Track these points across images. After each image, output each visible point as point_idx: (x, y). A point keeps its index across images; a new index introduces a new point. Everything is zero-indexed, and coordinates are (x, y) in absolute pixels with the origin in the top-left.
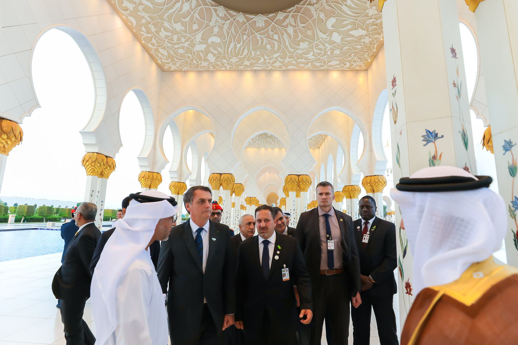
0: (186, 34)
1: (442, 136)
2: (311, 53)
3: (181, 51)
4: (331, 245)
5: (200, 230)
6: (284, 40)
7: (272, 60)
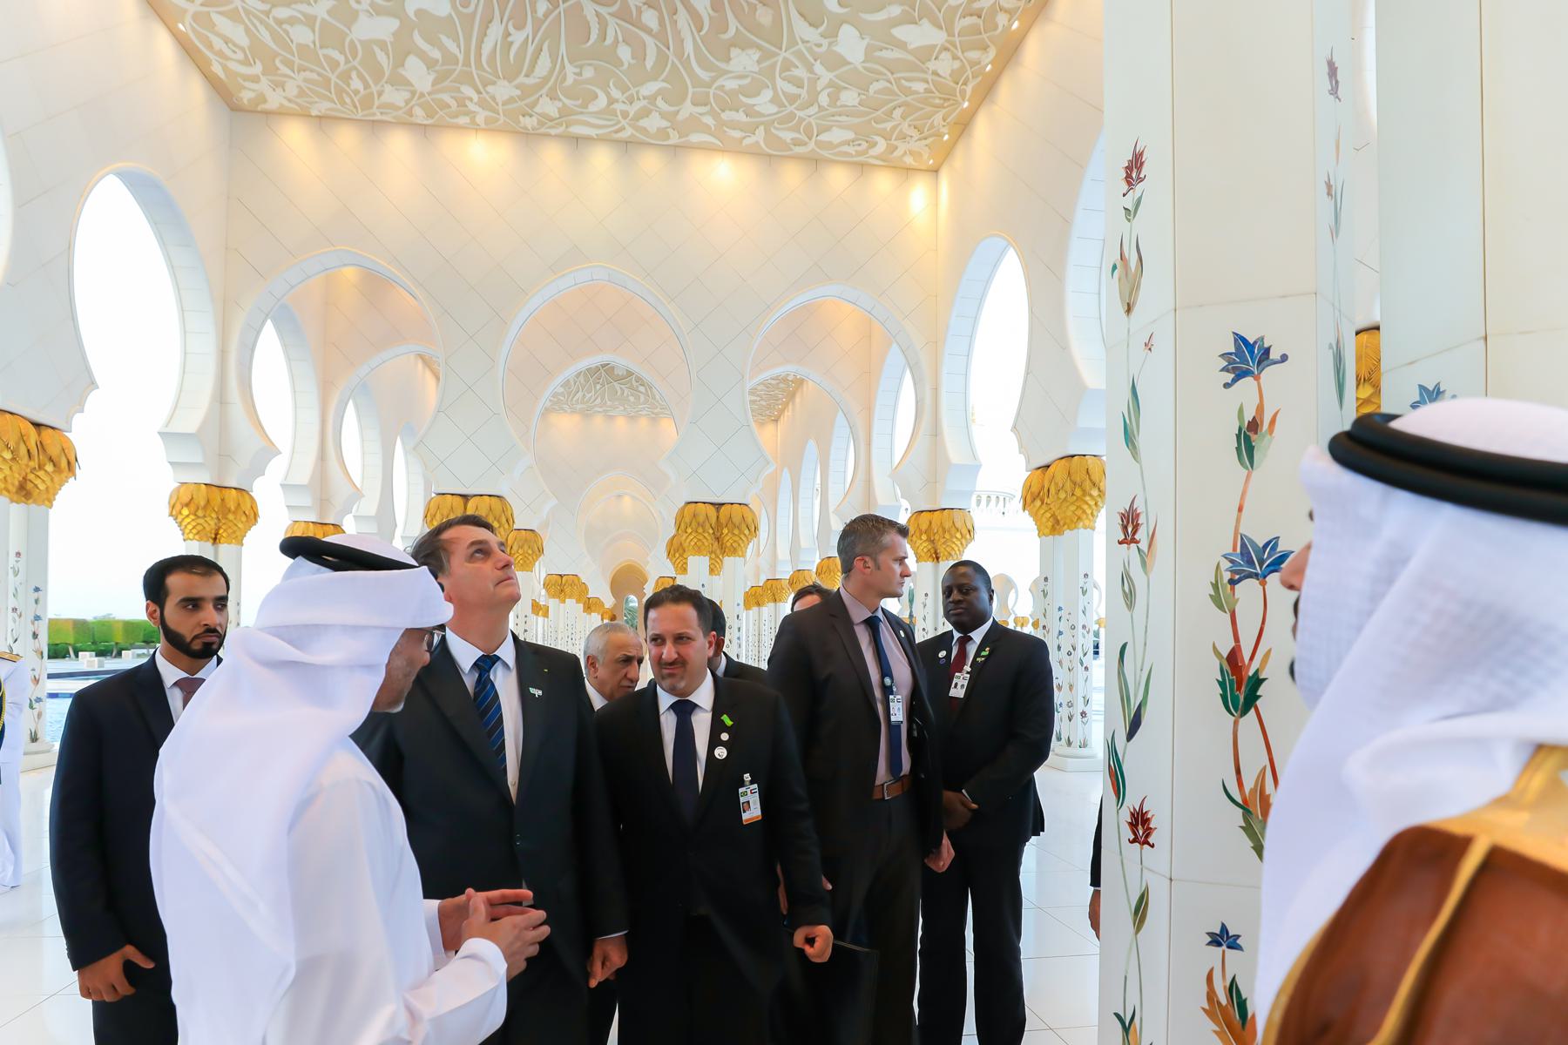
1: (1284, 358)
2: (767, 94)
4: (898, 712)
5: (486, 664)
6: (677, 33)
7: (638, 105)
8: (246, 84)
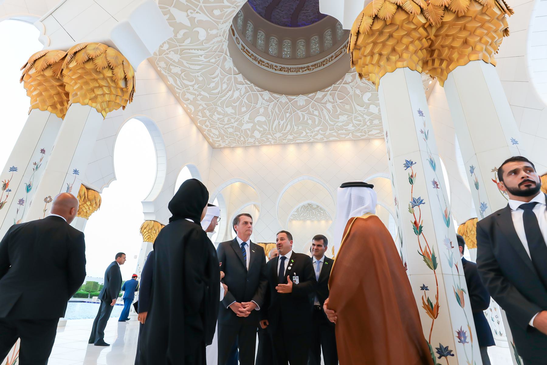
2: (351, 125)
3: (231, 130)
5: (244, 244)
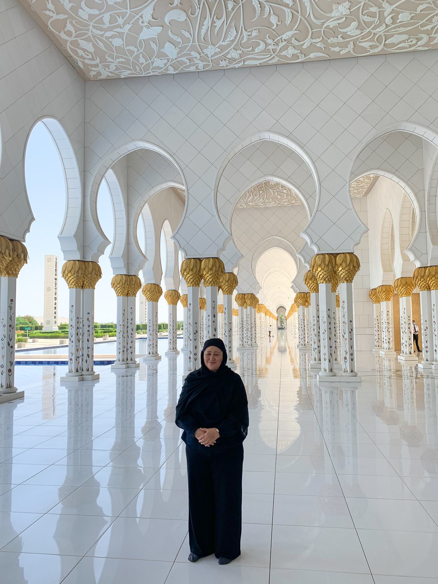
0: (125, 11)
2: (354, 24)
3: (117, 42)
8: (93, 69)
